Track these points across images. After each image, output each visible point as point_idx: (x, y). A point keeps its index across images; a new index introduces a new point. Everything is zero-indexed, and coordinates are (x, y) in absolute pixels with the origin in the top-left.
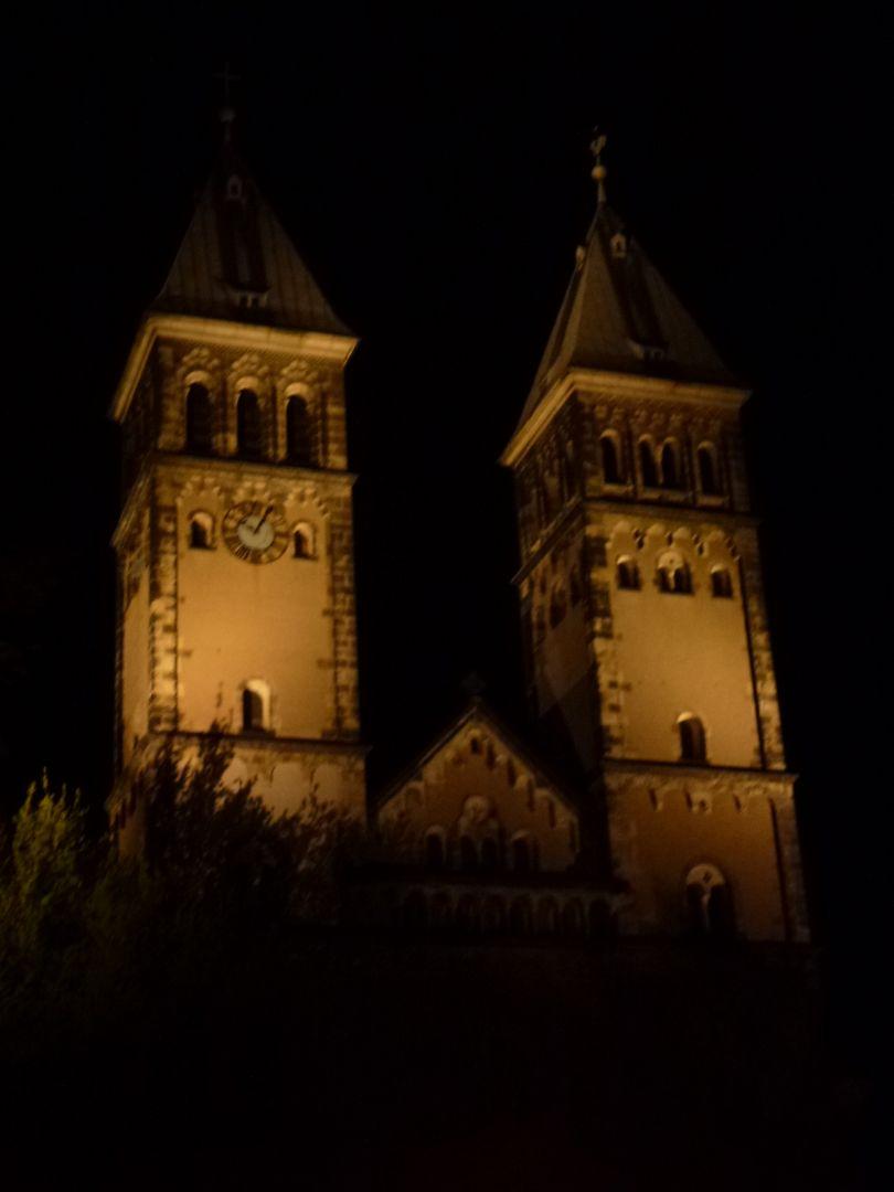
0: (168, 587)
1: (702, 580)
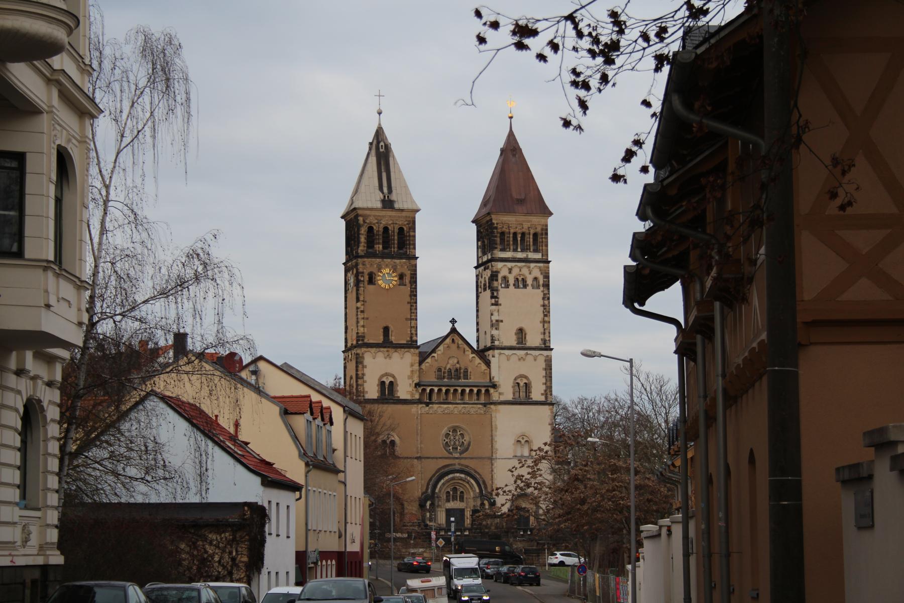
0: (361, 298)
1: (529, 281)
